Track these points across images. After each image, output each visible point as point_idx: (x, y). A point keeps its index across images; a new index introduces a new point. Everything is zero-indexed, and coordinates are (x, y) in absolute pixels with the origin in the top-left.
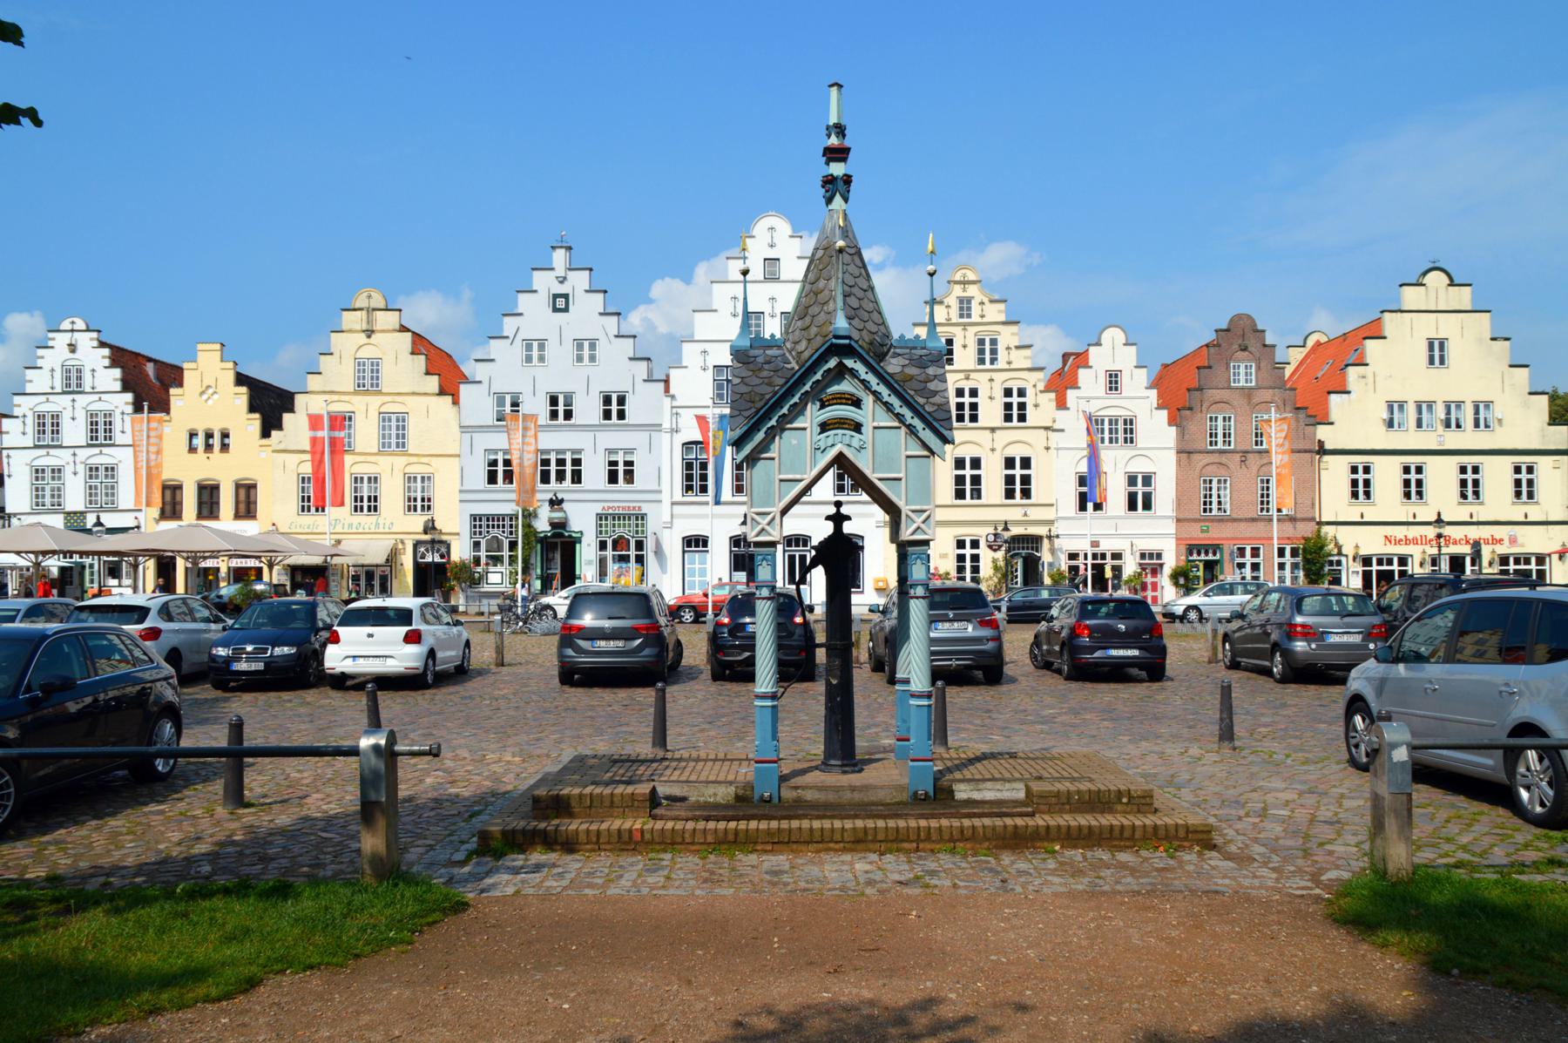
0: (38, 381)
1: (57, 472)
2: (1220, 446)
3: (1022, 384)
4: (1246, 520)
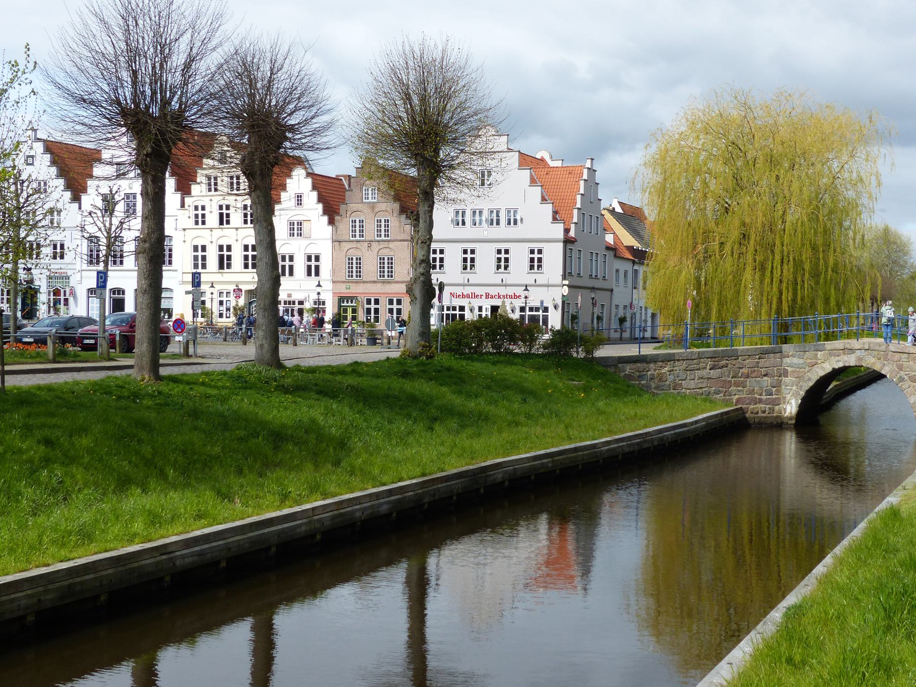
2: (358, 238)
3: (227, 203)
4: (371, 282)
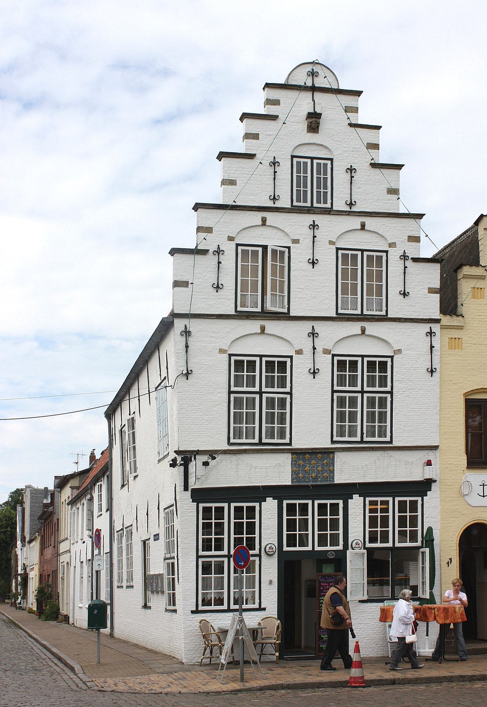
1: (278, 368)
2: (313, 505)
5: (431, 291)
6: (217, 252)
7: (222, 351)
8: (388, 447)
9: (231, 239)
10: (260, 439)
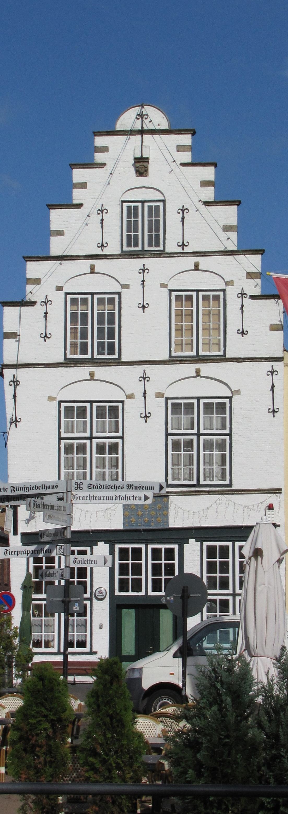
0: (71, 229)
2: (147, 550)
5: (273, 328)
6: (45, 302)
7: (51, 399)
8: (228, 490)
9: (59, 288)
10: (198, 480)
